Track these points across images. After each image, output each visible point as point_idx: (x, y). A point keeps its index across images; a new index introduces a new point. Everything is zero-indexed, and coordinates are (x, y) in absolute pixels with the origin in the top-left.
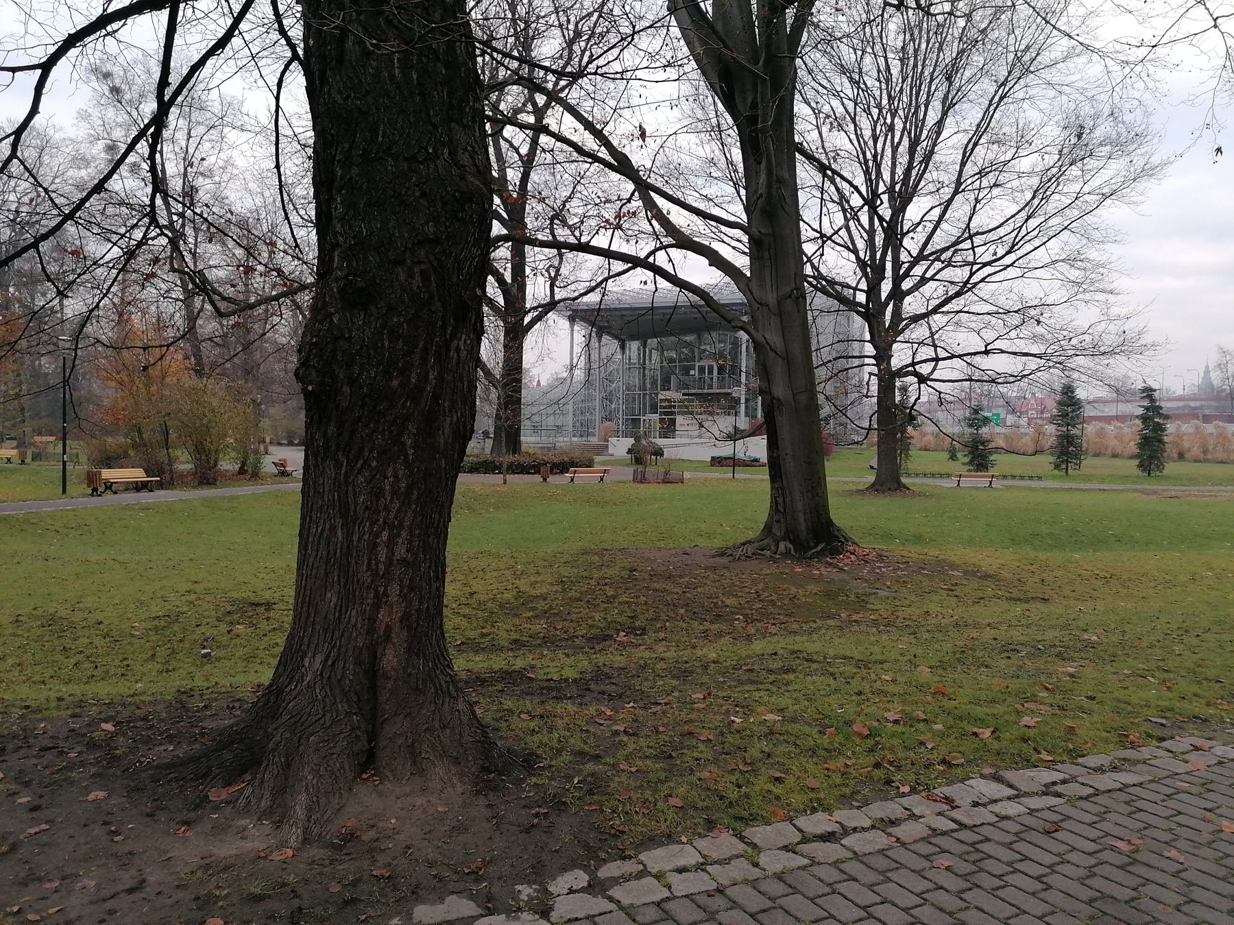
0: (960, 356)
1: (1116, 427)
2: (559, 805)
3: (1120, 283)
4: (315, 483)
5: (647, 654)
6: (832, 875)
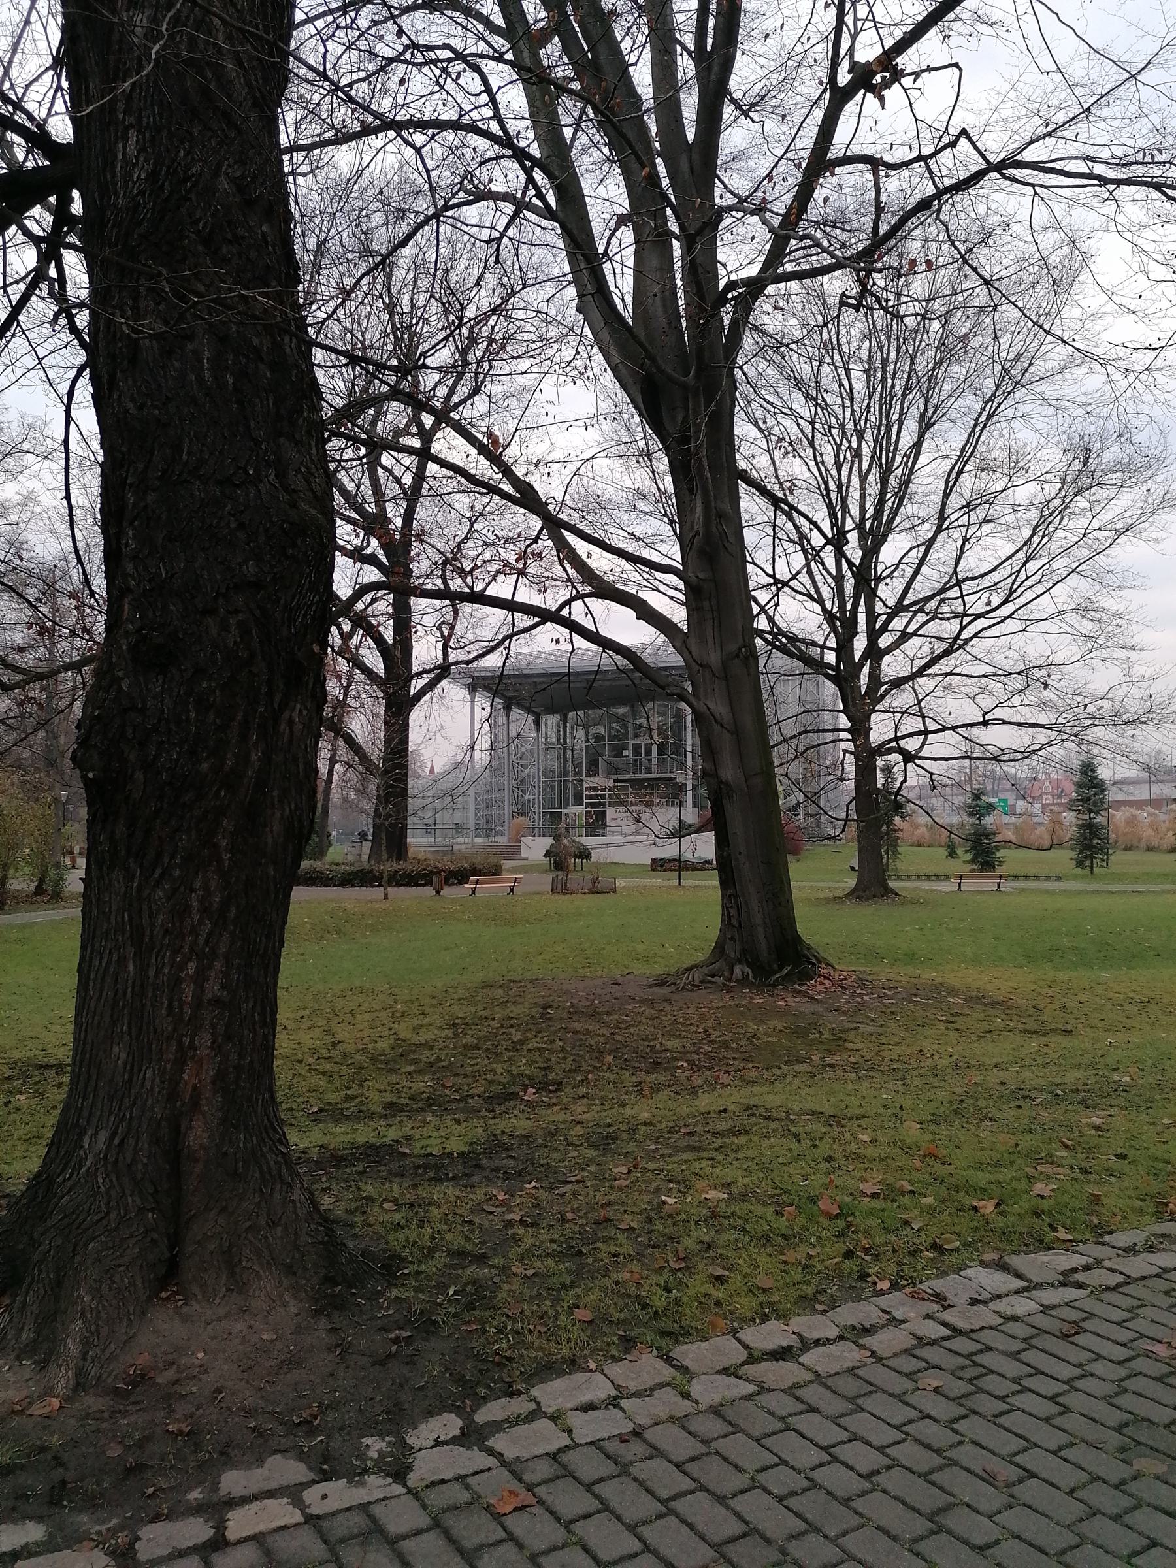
0: (953, 728)
1: (1150, 814)
2: (427, 1325)
3: (1143, 637)
4: (98, 900)
5: (561, 1117)
6: (783, 1404)
